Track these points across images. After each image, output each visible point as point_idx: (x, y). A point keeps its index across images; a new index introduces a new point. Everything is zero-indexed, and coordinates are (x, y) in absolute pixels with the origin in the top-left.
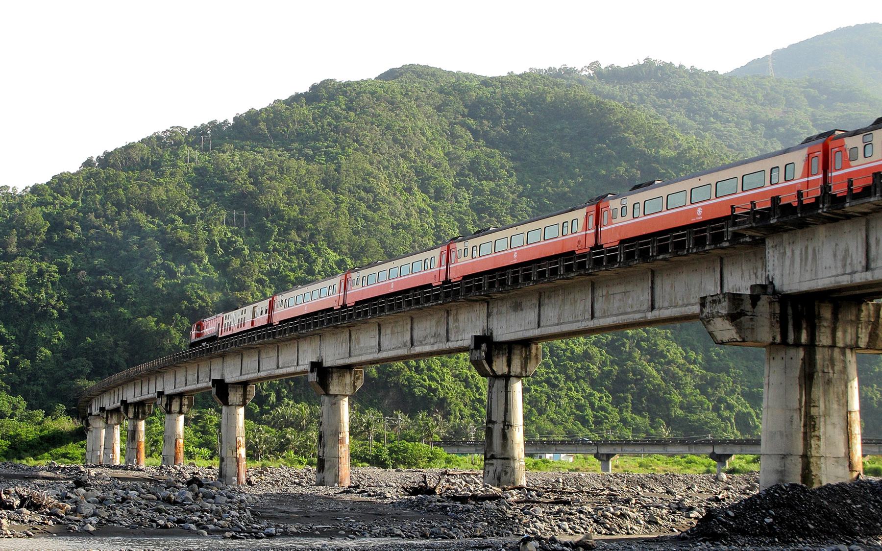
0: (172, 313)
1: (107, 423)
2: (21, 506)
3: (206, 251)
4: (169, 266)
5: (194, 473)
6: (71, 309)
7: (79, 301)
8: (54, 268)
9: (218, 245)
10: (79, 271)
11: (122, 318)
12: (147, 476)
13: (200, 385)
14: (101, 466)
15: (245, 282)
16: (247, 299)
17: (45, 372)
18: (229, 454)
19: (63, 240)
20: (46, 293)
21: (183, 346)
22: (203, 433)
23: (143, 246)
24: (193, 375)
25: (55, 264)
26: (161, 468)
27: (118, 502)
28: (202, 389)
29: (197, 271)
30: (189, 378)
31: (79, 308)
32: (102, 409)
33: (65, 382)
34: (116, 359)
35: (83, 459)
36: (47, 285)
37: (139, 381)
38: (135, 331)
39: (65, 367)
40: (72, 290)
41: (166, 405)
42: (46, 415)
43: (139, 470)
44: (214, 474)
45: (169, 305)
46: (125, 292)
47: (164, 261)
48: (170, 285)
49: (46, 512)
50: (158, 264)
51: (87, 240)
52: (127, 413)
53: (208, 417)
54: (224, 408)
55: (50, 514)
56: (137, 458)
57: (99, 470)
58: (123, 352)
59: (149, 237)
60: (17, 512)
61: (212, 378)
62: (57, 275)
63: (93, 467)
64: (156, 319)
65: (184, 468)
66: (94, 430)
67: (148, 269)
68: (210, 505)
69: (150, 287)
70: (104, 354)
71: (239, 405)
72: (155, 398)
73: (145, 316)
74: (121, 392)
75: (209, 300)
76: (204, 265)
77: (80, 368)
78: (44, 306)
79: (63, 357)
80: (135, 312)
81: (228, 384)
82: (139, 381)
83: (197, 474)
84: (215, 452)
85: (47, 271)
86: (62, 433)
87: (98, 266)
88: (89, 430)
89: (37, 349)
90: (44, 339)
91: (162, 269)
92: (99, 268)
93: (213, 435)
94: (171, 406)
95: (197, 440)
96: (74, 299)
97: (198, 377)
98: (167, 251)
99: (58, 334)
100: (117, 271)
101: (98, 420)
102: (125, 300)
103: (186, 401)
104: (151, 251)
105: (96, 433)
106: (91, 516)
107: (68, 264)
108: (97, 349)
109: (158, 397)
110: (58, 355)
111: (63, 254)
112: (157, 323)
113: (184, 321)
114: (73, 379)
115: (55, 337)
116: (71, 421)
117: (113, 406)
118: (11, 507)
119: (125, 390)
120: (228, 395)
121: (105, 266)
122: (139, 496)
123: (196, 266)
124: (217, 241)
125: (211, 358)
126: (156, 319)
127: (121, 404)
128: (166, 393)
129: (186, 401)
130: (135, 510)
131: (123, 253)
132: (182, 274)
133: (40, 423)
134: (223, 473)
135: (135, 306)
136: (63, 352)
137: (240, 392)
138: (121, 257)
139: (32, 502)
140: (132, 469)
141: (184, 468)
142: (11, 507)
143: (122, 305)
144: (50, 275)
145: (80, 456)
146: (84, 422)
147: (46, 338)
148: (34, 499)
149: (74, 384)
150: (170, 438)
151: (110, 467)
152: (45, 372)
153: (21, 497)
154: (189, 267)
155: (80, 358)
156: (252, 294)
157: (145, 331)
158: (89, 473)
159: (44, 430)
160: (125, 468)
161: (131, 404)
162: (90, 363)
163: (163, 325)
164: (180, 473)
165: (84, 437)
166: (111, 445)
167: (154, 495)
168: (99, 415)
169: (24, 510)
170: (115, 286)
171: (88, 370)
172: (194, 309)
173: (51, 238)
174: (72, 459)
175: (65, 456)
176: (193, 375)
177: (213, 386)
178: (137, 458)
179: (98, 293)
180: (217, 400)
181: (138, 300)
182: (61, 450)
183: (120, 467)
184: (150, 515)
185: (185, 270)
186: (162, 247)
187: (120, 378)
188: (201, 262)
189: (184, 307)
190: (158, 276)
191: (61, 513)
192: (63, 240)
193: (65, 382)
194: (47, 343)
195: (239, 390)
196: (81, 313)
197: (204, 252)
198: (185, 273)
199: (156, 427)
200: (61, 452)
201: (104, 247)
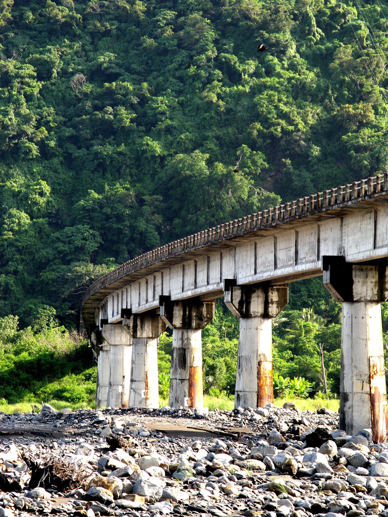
0: (236, 145)
1: (134, 336)
2: (32, 485)
3: (293, 33)
4: (228, 62)
5: (295, 422)
6: (61, 141)
7: (74, 126)
8: (29, 70)
9: (314, 22)
10: (73, 74)
11: (149, 155)
12: (212, 427)
13: (301, 268)
14: (132, 410)
15: (362, 86)
16: (365, 116)
17: (19, 251)
18: (357, 387)
19: (43, 19)
20: (17, 114)
21: (255, 201)
22: (296, 351)
23: (181, 28)
24: (288, 249)
25: (30, 63)
26: (236, 412)
27: (200, 473)
28: (303, 274)
29: (278, 69)
30: (281, 255)
31: (74, 140)
32: (126, 313)
33: (55, 267)
34: (142, 225)
35: (90, 401)
36: (18, 100)
37: (192, 263)
38: (172, 178)
39: (54, 242)
40: (62, 107)
41: (241, 303)
42: (22, 325)
43: (197, 417)
44: (331, 424)
45: (230, 130)
46: (153, 109)
47: (219, 53)
48: (230, 95)
49: (79, 494)
50: (209, 60)
51: (85, 19)
52: (170, 317)
53: (303, 323)
54: (346, 307)
55: (88, 498)
56: (190, 395)
57: (129, 418)
58: (153, 213)
59: (192, 11)
60: (28, 495)
61: (323, 254)
62: (34, 83)
63: (116, 413)
64: (207, 156)
65: (276, 414)
66: (112, 350)
67: (192, 69)
68: (363, 479)
69: (197, 100)
70: (119, 218)
71: (372, 301)
72: (220, 292)
73: (187, 151)
74: (158, 282)
75: (298, 120)
76: (289, 59)
77: (78, 243)
78: (14, 137)
79: (50, 224)
80: (171, 144)
81: (351, 264)
82: (192, 263)
83: (300, 423)
84: (317, 385)
85: (17, 76)
86: (52, 355)
87: (105, 65)
88: (101, 349)
89: (4, 211)
90: (15, 195)
91: (216, 67)
92: (106, 69)
93: (311, 355)
94: (248, 304)
95: (285, 364)
96: (65, 124)
97: (297, 252)
98: (223, 35)
99: (39, 184)
100: (138, 73)
101: (118, 331)
102: (154, 124)
103: (274, 296)
104: (197, 37)
105: (115, 354)
106: (160, 501)
107: (53, 63)
108: (108, 210)
109: (227, 289)
110: (41, 220)
111: (45, 44)
112: (210, 163)
113: (256, 158)
114: (68, 263)
115: (34, 190)
116: (67, 334)
117: (144, 307)
118: (15, 487)
119: (166, 279)
120: (352, 283)
121: (117, 64)
122: (232, 462)
123: (276, 60)
124: (311, 14)
125: (319, 219)
126: (207, 156)
127: (161, 304)
128: (241, 281)
129: (274, 296)
130: (235, 489)
131: (149, 41)
132: (251, 76)
133: (13, 340)
134: (348, 420)
135: (171, 134)
136: (49, 215)
137: (373, 278)
138: (145, 48)
139: (53, 476)
140: (186, 416)
141: (276, 414)
142: (15, 487)
143: (148, 132)
144: (22, 83)
145: (85, 395)
146: (93, 336)
147: (20, 192)
148: (57, 469)
149: (70, 271)
150: (248, 359)
151: (145, 412)
152: (19, 251)
153: (33, 466)
154: (262, 62)
155: (80, 226)
156: (375, 108)
157: (191, 176)
158: (113, 423)
159: (22, 350)
160: (173, 414)
161: (177, 302)
162: (97, 233)
163: (220, 167)
164: (270, 421)
165: (93, 363)
166: (143, 375)
167: (261, 460)
168: (120, 323)
169: (41, 491)
170: (135, 100)
171: (92, 246)
172: (272, 137)
173: (22, 17)
174: (72, 400)
175: (59, 395)
176: (288, 249)
177: (325, 268)
178: (190, 395)
179: (106, 113)
180: (333, 292)
181: (175, 123)
182: (54, 386)
183: (156, 413)
184: (261, 497)
185: (257, 67)
186: (216, 29)
187: (157, 258)
188: (284, 52)
189: (255, 132)
190: (209, 80)
191: (107, 494)
192: (43, 19)
193: (55, 267)
194: (21, 200)
195: (371, 274)
196: (79, 148)
197: (288, 36)
198: (256, 74)
199: (213, 342)
200: (53, 388)
201: (114, 32)
